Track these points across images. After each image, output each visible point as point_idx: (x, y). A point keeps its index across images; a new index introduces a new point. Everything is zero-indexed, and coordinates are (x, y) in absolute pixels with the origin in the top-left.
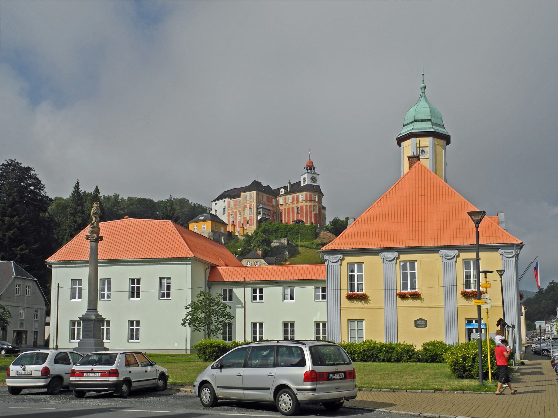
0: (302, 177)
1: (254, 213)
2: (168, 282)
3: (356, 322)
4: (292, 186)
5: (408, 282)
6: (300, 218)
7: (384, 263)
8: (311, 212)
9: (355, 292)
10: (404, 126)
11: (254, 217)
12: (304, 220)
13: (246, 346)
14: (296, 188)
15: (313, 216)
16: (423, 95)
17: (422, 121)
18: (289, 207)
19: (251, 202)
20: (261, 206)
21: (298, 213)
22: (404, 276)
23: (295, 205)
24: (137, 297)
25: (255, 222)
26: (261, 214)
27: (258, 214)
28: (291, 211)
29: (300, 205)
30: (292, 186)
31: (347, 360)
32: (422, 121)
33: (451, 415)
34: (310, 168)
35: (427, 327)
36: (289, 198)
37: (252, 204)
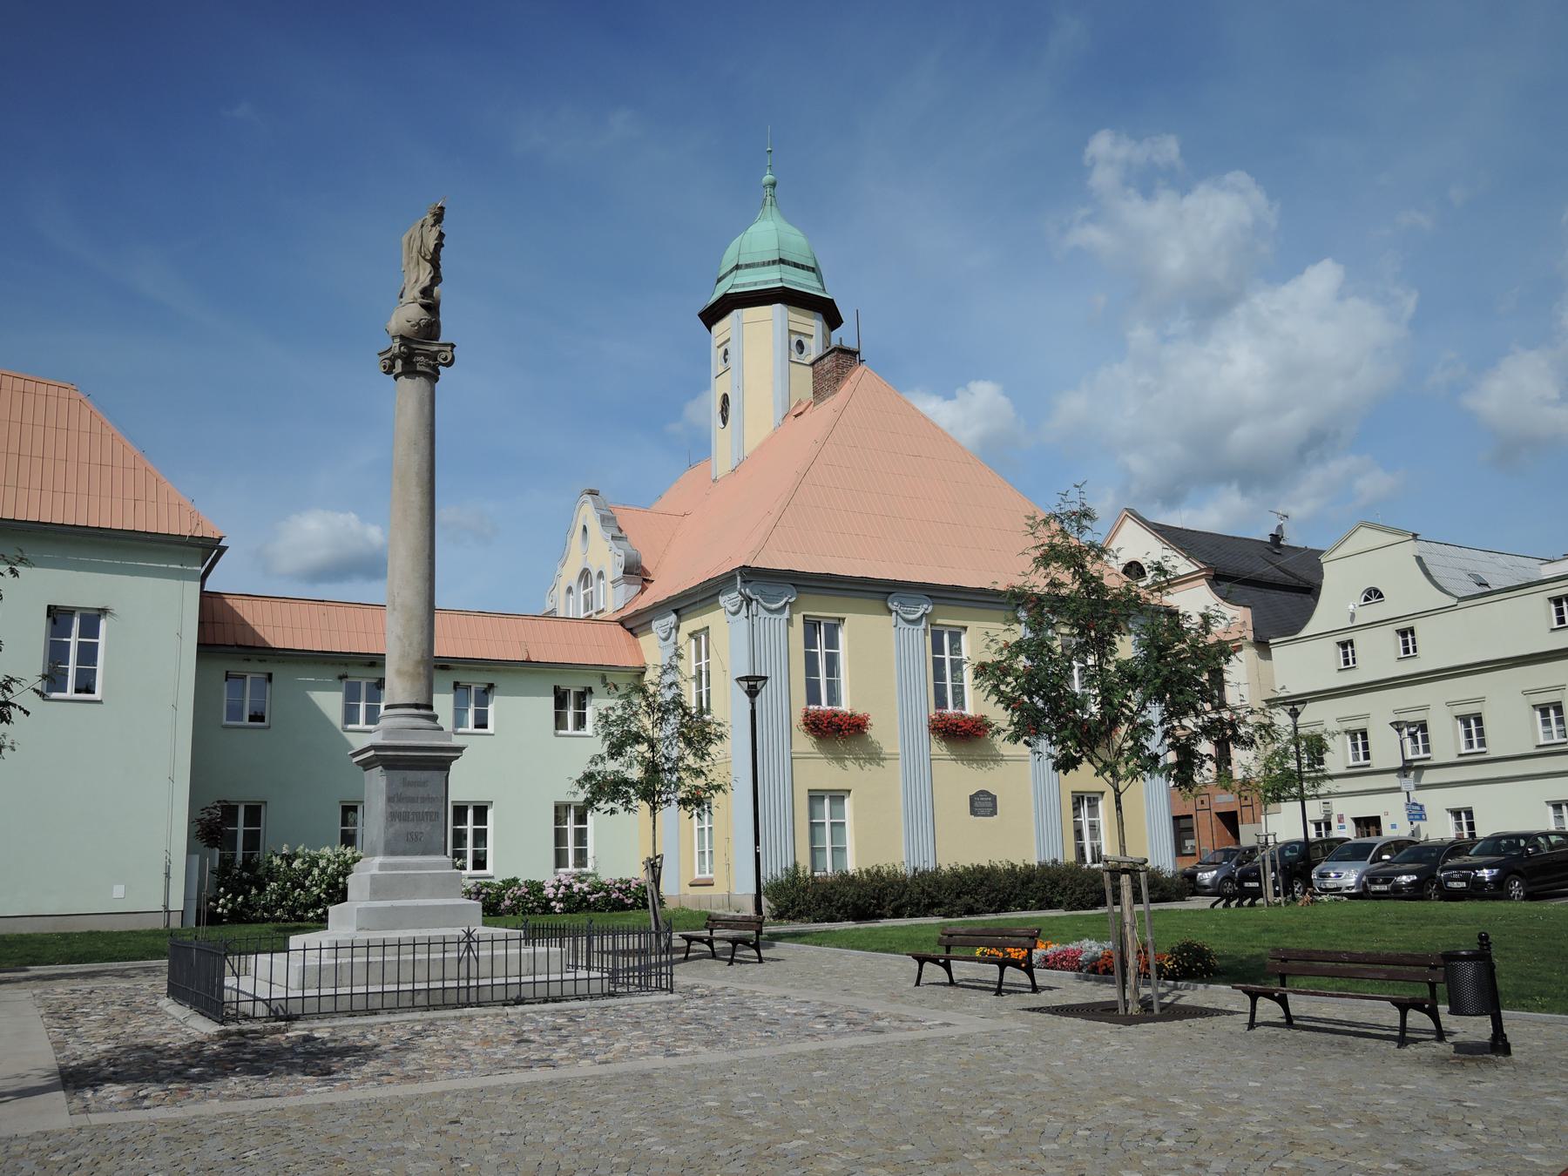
2: (440, 650)
3: (827, 801)
5: (96, 644)
7: (899, 626)
9: (816, 707)
13: (1023, 916)
16: (774, 204)
17: (796, 265)
22: (811, 661)
32: (796, 265)
33: (431, 1024)
35: (996, 814)
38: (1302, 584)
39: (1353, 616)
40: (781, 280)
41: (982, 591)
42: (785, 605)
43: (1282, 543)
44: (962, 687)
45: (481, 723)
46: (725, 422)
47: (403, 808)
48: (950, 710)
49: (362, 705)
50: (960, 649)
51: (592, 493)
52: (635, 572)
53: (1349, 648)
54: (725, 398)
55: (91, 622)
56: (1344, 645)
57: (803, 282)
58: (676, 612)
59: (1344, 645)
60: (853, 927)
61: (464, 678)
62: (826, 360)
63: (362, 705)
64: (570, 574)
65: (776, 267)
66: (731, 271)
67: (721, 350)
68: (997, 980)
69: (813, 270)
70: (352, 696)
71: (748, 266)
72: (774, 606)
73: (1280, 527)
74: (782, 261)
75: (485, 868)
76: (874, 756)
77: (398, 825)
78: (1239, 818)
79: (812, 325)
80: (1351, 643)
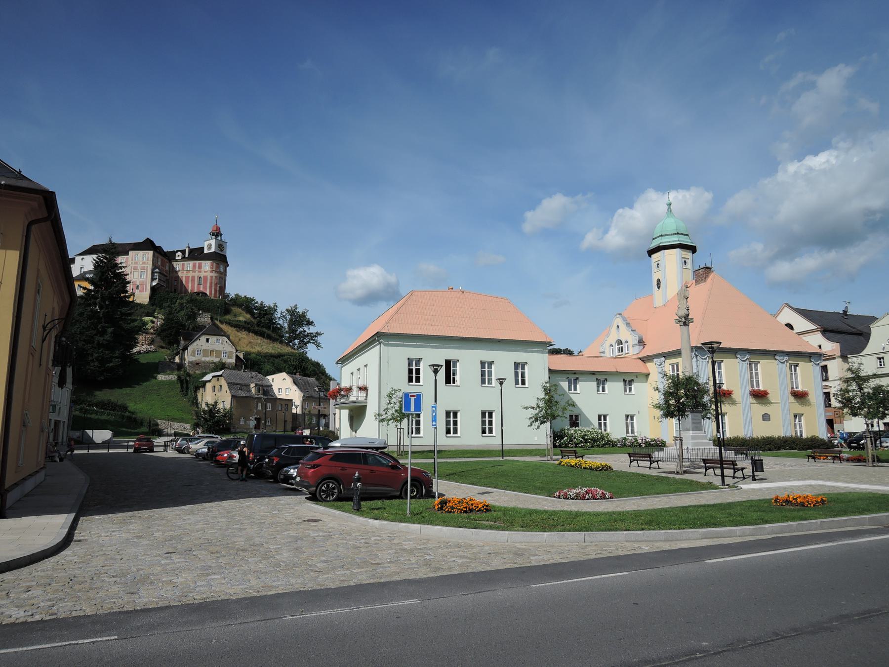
0: (206, 242)
1: (146, 277)
4: (191, 251)
6: (202, 289)
8: (216, 284)
10: (654, 239)
11: (146, 281)
12: (208, 293)
14: (196, 254)
15: (218, 289)
17: (683, 234)
18: (188, 275)
19: (144, 263)
20: (157, 270)
21: (199, 284)
23: (197, 274)
24: (489, 433)
25: (149, 288)
26: (157, 280)
27: (153, 279)
28: (190, 281)
29: (203, 274)
30: (191, 251)
31: (72, 431)
32: (683, 234)
34: (217, 234)
36: (189, 265)
37: (146, 266)
38: (858, 332)
39: (884, 348)
40: (679, 240)
41: (765, 351)
42: (706, 358)
43: (847, 313)
44: (758, 381)
45: (575, 389)
46: (659, 288)
47: (694, 421)
48: (755, 388)
49: (573, 385)
50: (757, 369)
51: (620, 314)
52: (641, 342)
53: (882, 360)
54: (659, 281)
55: (523, 365)
56: (880, 359)
57: (685, 241)
58: (664, 357)
59: (880, 359)
60: (387, 471)
61: (599, 377)
62: (701, 271)
63: (573, 385)
64: (612, 339)
65: (676, 235)
66: (659, 236)
67: (656, 263)
68: (752, 474)
69: (688, 235)
70: (570, 383)
71: (666, 235)
72: (704, 357)
73: (847, 307)
74: (678, 233)
75: (420, 434)
76: (734, 403)
77: (694, 425)
78: (834, 422)
79: (688, 254)
80: (883, 358)
